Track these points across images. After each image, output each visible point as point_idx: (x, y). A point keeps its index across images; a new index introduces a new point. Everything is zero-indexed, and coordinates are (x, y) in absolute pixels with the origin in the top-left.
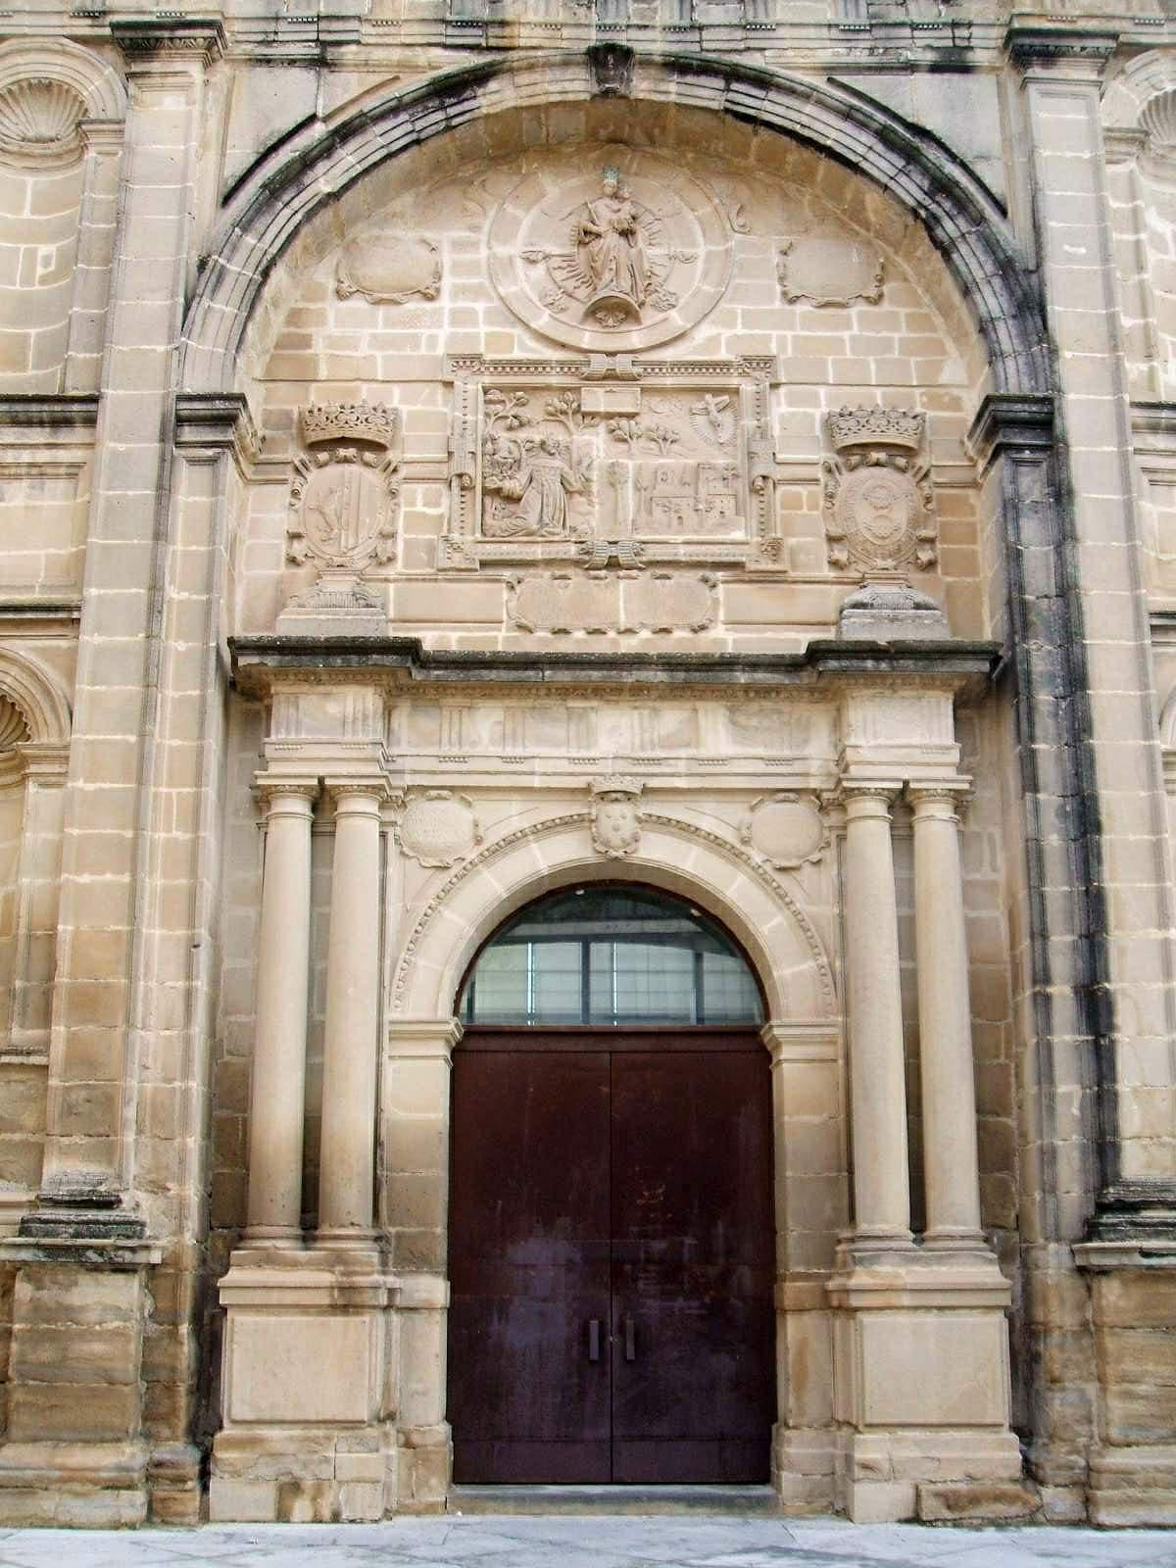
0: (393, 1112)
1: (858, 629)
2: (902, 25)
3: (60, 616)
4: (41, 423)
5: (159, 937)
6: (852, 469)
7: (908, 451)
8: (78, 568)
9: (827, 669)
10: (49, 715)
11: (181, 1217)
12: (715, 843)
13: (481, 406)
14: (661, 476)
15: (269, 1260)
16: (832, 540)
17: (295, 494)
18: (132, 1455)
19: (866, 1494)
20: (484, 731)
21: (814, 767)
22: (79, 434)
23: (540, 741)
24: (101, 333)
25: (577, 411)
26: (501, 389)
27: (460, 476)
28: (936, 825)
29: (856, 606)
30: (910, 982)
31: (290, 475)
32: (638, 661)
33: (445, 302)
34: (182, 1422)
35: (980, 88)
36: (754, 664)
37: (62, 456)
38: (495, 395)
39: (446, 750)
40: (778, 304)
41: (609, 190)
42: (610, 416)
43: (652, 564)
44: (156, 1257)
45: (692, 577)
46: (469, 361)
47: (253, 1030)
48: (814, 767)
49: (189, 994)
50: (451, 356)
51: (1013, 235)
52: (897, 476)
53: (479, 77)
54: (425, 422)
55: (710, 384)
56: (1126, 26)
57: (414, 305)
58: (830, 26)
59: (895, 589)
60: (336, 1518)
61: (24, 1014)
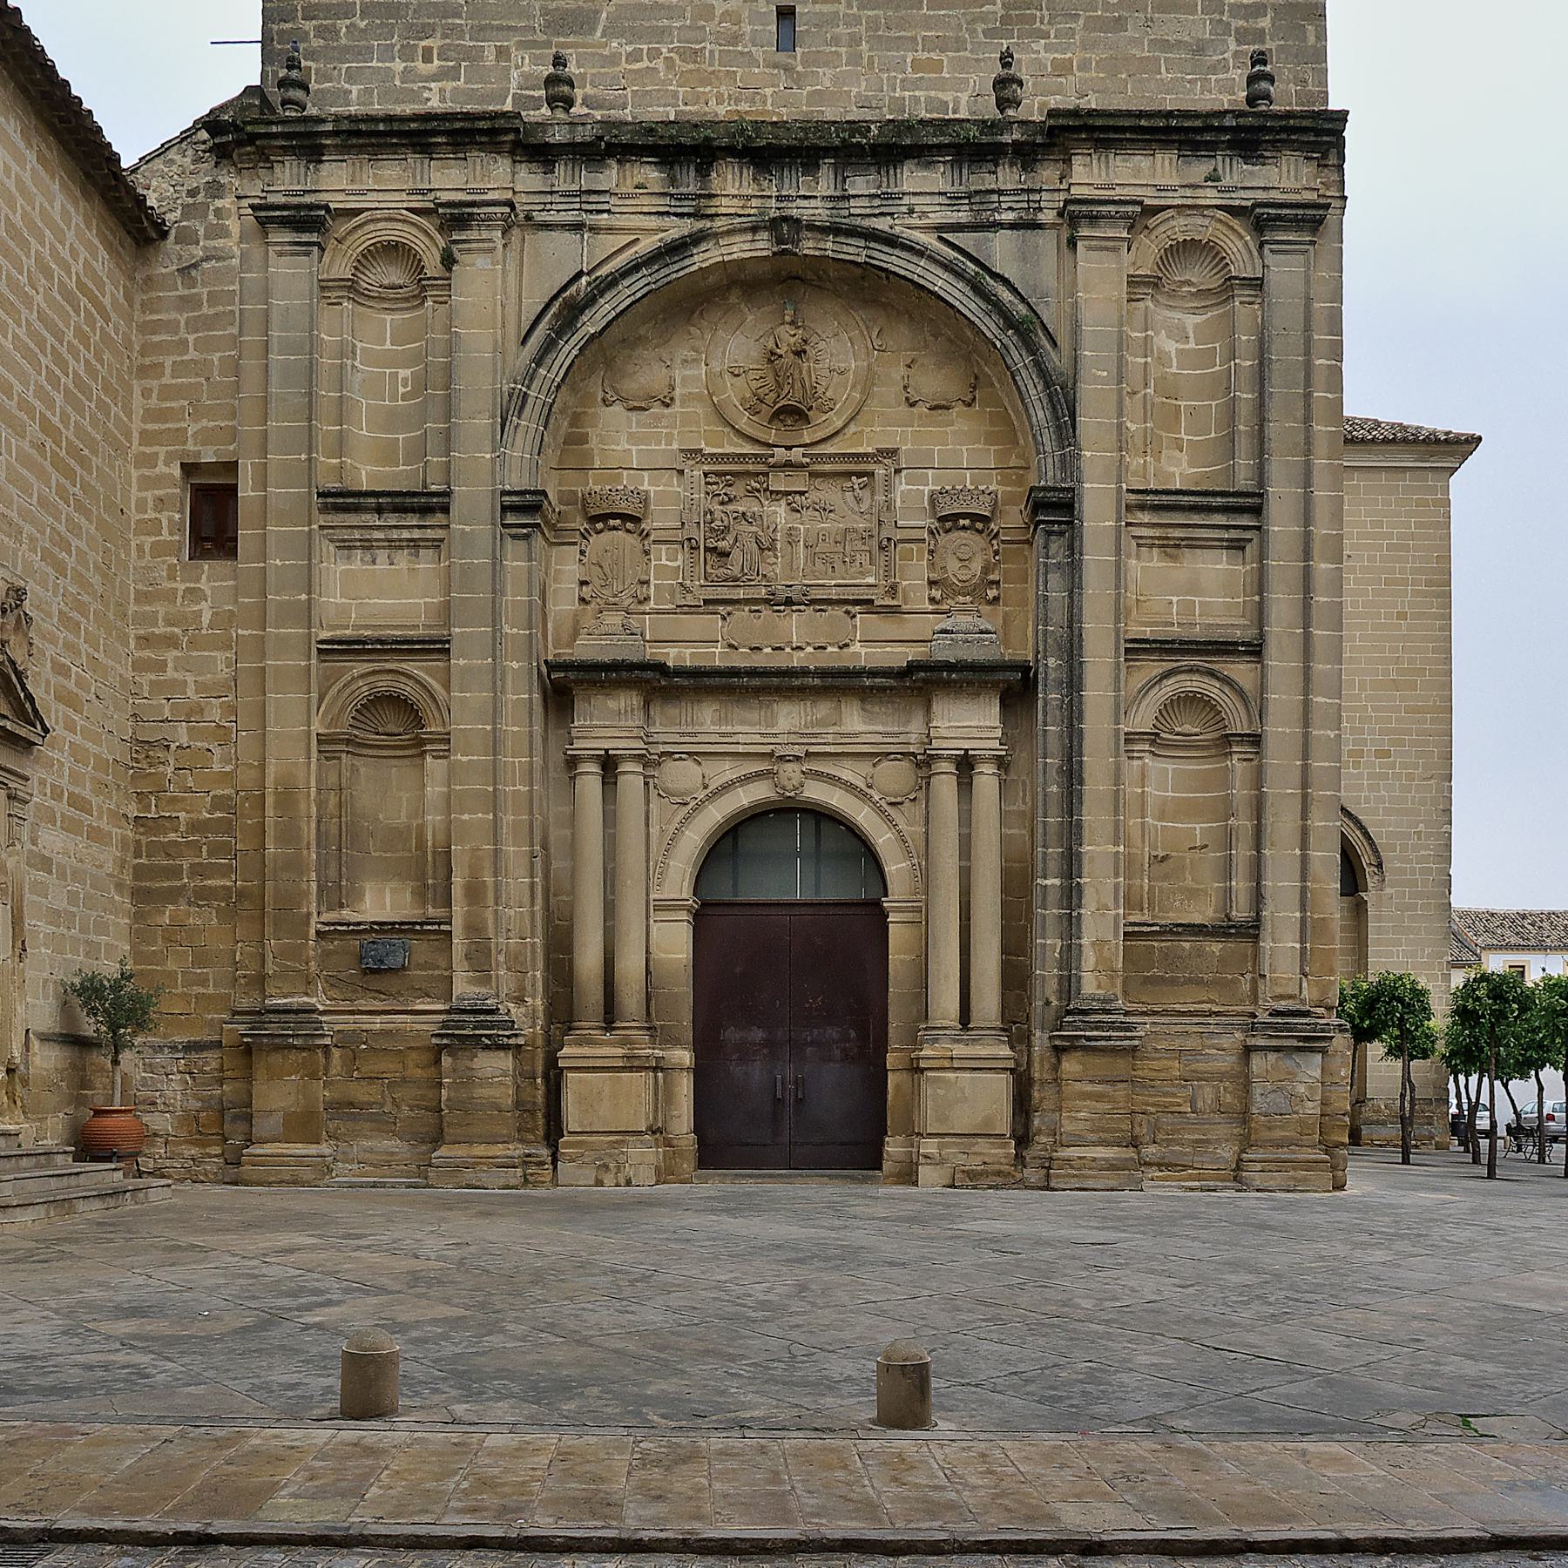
0: (656, 954)
1: (945, 652)
2: (992, 192)
3: (437, 647)
4: (413, 511)
5: (514, 851)
6: (947, 532)
7: (985, 520)
8: (446, 611)
9: (921, 682)
10: (437, 715)
11: (534, 1019)
12: (851, 788)
13: (703, 488)
14: (823, 537)
15: (590, 1042)
16: (932, 583)
17: (582, 553)
18: (516, 1150)
19: (924, 1172)
20: (708, 720)
21: (913, 738)
22: (439, 518)
23: (743, 723)
24: (448, 440)
25: (766, 490)
26: (717, 474)
27: (689, 539)
28: (986, 780)
29: (942, 632)
30: (966, 876)
31: (578, 539)
32: (804, 672)
33: (677, 408)
34: (541, 1133)
35: (1047, 242)
36: (873, 673)
37: (430, 534)
38: (713, 479)
39: (684, 729)
40: (904, 408)
41: (787, 319)
42: (788, 493)
43: (813, 602)
44: (521, 1041)
45: (838, 612)
46: (693, 453)
47: (571, 905)
48: (913, 738)
49: (532, 885)
50: (682, 451)
51: (1057, 361)
52: (977, 538)
53: (697, 239)
54: (669, 498)
55: (857, 471)
56: (1151, 192)
57: (656, 409)
58: (940, 193)
59: (970, 619)
60: (628, 1183)
61: (434, 900)
